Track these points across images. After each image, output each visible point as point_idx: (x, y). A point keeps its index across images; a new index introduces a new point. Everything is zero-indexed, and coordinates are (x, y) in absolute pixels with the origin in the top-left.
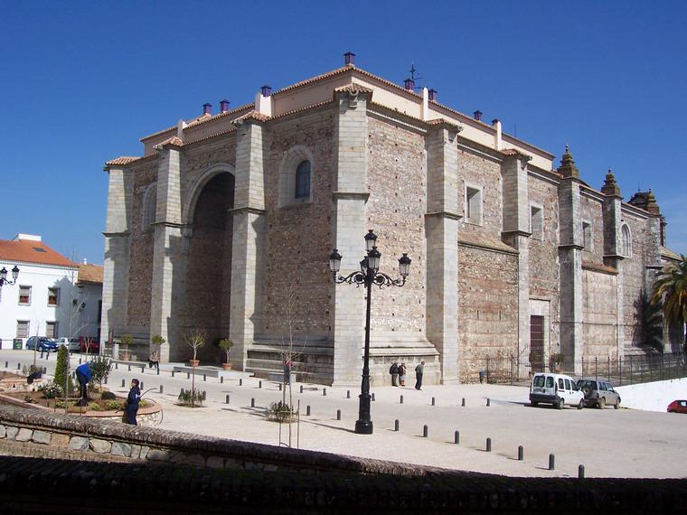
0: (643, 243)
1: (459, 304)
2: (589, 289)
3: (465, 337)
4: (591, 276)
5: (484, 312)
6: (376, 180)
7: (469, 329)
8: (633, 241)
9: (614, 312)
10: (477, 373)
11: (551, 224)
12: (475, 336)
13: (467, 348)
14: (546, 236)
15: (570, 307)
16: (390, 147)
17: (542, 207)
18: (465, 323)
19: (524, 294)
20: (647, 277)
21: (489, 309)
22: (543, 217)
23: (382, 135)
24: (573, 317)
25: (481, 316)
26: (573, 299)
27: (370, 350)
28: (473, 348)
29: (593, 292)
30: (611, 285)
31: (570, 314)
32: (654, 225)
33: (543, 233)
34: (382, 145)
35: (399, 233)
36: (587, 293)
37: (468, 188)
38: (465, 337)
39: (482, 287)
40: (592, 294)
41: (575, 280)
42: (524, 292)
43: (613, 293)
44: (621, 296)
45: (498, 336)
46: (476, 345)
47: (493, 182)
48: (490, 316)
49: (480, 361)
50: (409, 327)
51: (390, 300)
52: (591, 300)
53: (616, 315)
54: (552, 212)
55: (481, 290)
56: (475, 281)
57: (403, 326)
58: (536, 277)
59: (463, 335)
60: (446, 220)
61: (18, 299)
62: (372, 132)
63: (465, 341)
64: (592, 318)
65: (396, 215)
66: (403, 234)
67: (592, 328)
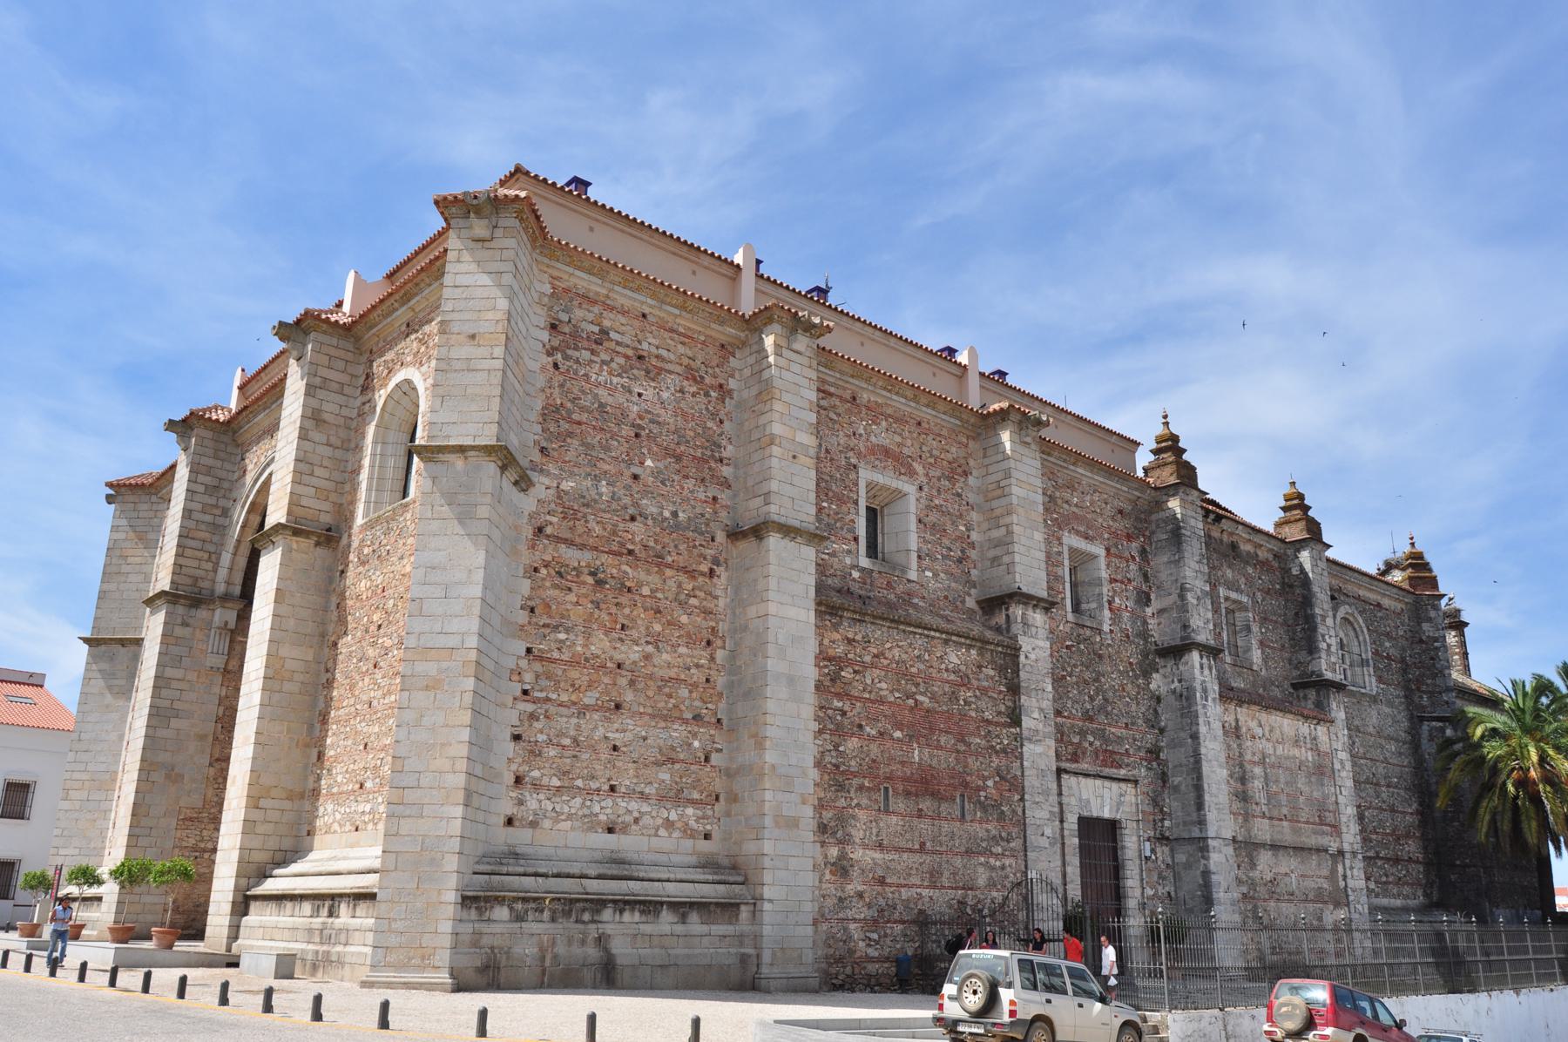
0: (1403, 660)
1: (818, 764)
2: (1248, 757)
3: (842, 856)
4: (1253, 724)
5: (908, 794)
6: (570, 434)
7: (857, 835)
8: (1376, 653)
9: (1330, 818)
10: (887, 959)
11: (1133, 595)
12: (878, 855)
13: (851, 888)
14: (1116, 618)
15: (1192, 795)
16: (622, 361)
17: (1099, 550)
18: (842, 819)
19: (1039, 754)
20: (1424, 741)
21: (924, 785)
22: (1104, 574)
23: (596, 329)
24: (1202, 822)
25: (899, 804)
26: (1200, 777)
27: (1052, 944)
28: (870, 892)
29: (1262, 762)
30: (1315, 749)
31: (1194, 816)
32: (1430, 620)
33: (1107, 613)
34: (593, 352)
35: (642, 576)
36: (1241, 766)
37: (1070, 548)
38: (842, 856)
39: (899, 726)
40: (1258, 770)
41: (1203, 729)
42: (1039, 749)
43: (1322, 771)
44: (1346, 778)
45: (958, 862)
46: (882, 881)
47: (950, 479)
48: (926, 804)
49: (899, 928)
50: (669, 824)
51: (604, 749)
52: (1257, 784)
53: (1336, 829)
54: (1133, 567)
55: (898, 734)
56: (874, 708)
57: (646, 820)
58: (1091, 719)
59: (834, 852)
60: (774, 541)
61: (511, 829)
62: (564, 317)
63: (842, 869)
64: (1262, 830)
65: (634, 527)
66: (655, 579)
67: (1264, 858)
